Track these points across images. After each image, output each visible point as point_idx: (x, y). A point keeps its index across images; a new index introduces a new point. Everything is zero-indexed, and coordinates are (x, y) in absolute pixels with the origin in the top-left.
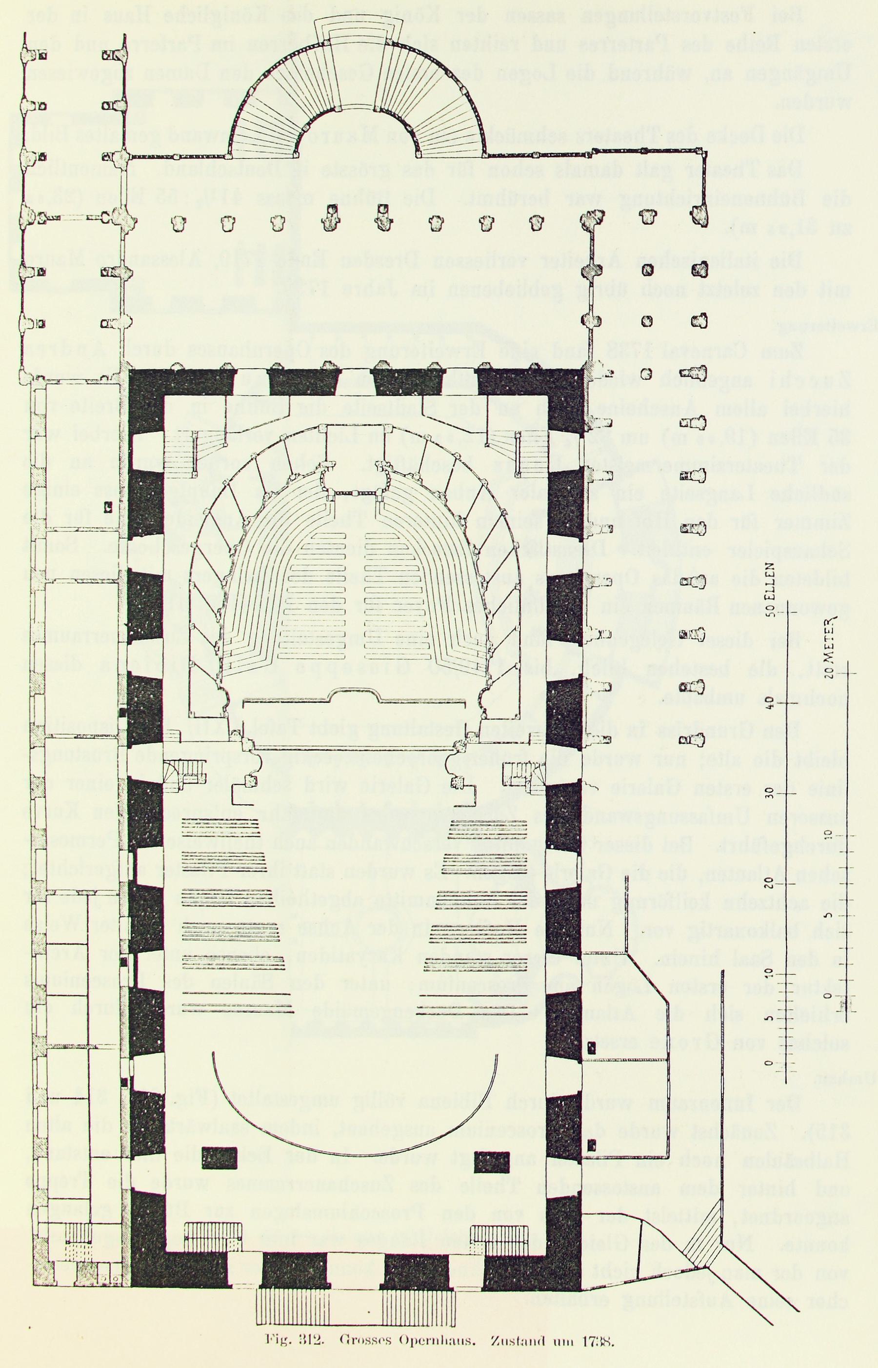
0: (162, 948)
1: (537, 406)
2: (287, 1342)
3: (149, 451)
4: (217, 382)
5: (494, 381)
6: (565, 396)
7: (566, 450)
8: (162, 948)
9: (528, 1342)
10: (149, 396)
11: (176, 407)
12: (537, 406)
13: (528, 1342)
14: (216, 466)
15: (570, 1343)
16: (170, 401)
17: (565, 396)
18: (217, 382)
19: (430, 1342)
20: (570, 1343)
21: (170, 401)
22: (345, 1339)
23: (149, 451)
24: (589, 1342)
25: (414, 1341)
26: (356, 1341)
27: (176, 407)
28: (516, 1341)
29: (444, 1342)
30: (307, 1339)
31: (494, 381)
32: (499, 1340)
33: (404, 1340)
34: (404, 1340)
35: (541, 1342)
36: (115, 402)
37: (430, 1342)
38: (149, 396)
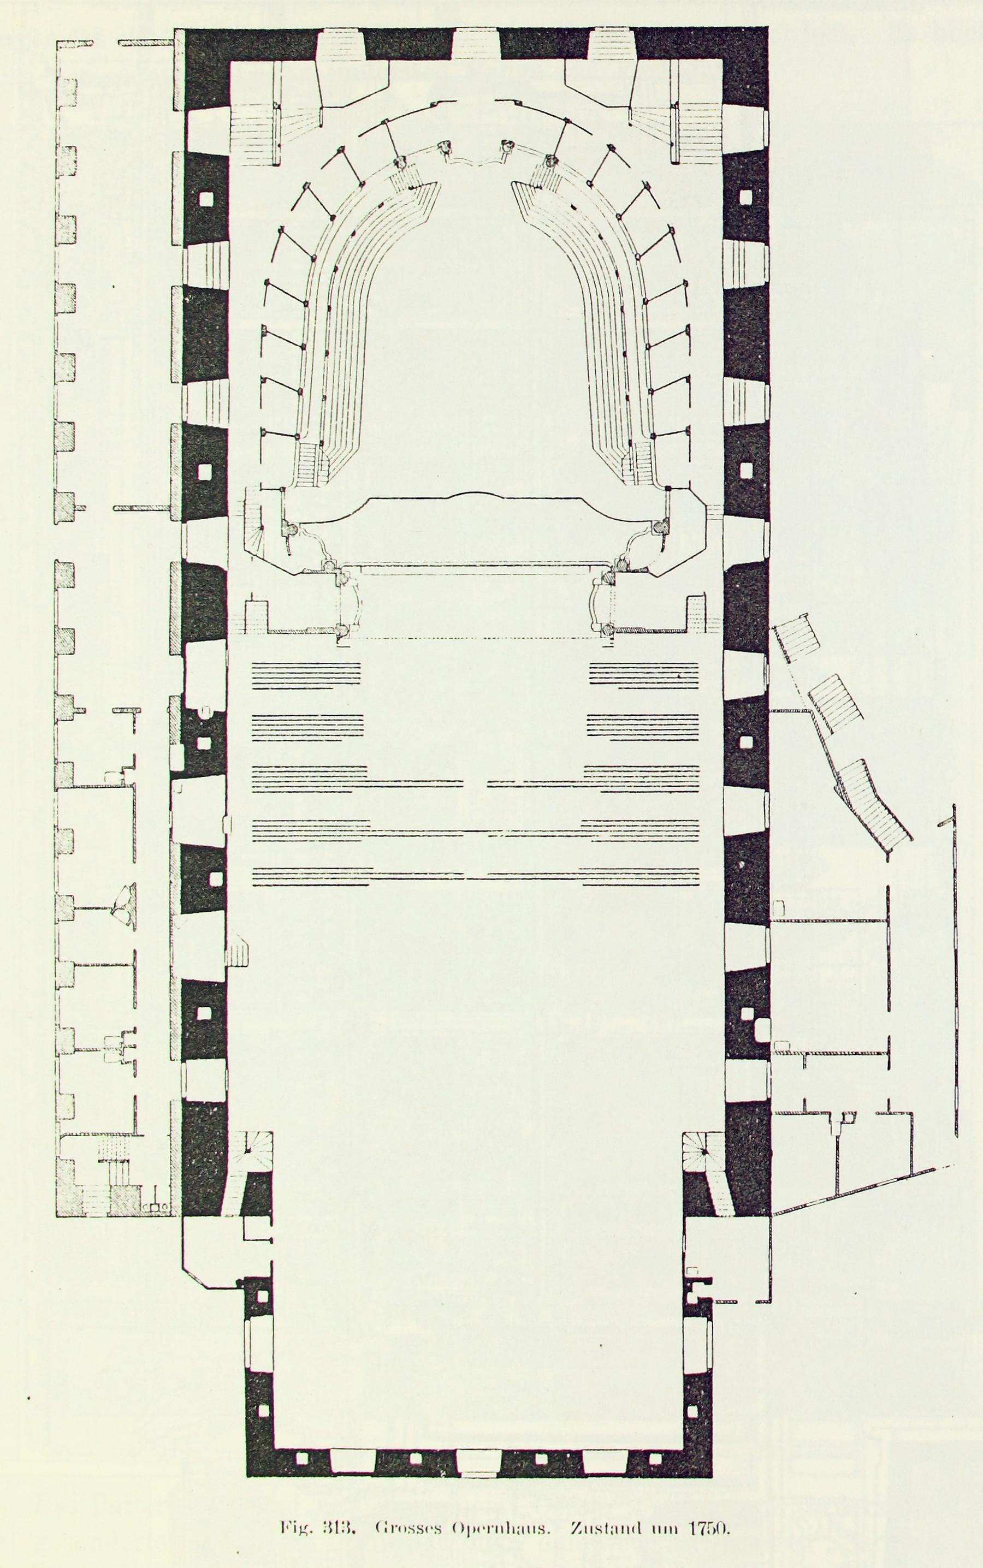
0: (727, 839)
1: (706, 74)
2: (308, 1530)
3: (210, 131)
4: (297, 44)
5: (656, 43)
6: (744, 61)
7: (743, 129)
8: (727, 839)
9: (526, 1530)
10: (210, 64)
11: (246, 76)
12: (706, 74)
13: (526, 1530)
14: (305, 151)
15: (657, 1530)
16: (237, 68)
17: (744, 61)
18: (297, 44)
19: (493, 1530)
20: (657, 1530)
21: (237, 68)
22: (382, 1527)
23: (210, 131)
24: (698, 1529)
25: (471, 1530)
26: (396, 1529)
27: (246, 76)
28: (603, 1529)
29: (511, 1530)
30: (333, 1526)
31: (656, 43)
32: (581, 1528)
33: (458, 1528)
34: (458, 1528)
35: (636, 1529)
36: (167, 70)
37: (493, 1530)
38: (210, 64)
